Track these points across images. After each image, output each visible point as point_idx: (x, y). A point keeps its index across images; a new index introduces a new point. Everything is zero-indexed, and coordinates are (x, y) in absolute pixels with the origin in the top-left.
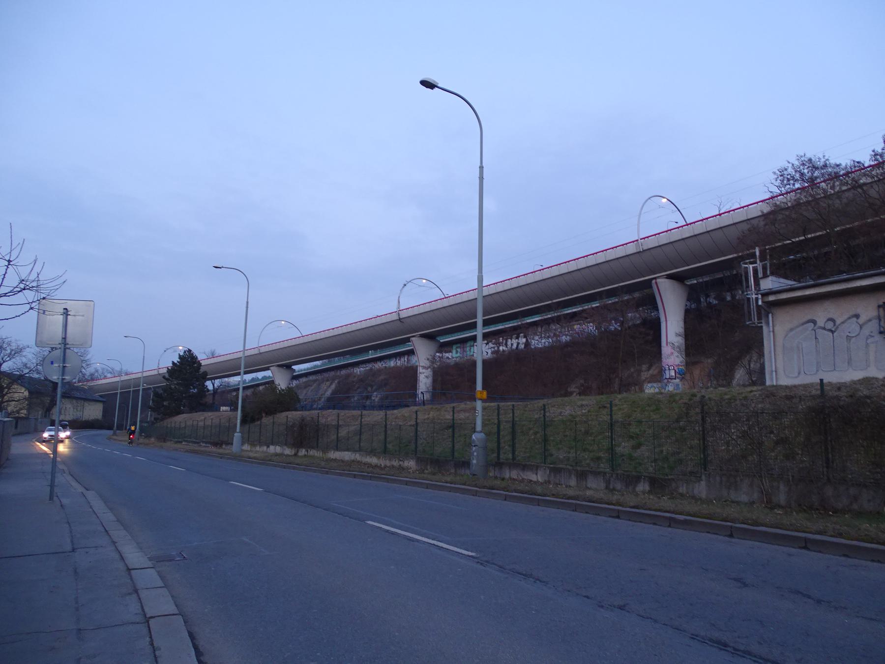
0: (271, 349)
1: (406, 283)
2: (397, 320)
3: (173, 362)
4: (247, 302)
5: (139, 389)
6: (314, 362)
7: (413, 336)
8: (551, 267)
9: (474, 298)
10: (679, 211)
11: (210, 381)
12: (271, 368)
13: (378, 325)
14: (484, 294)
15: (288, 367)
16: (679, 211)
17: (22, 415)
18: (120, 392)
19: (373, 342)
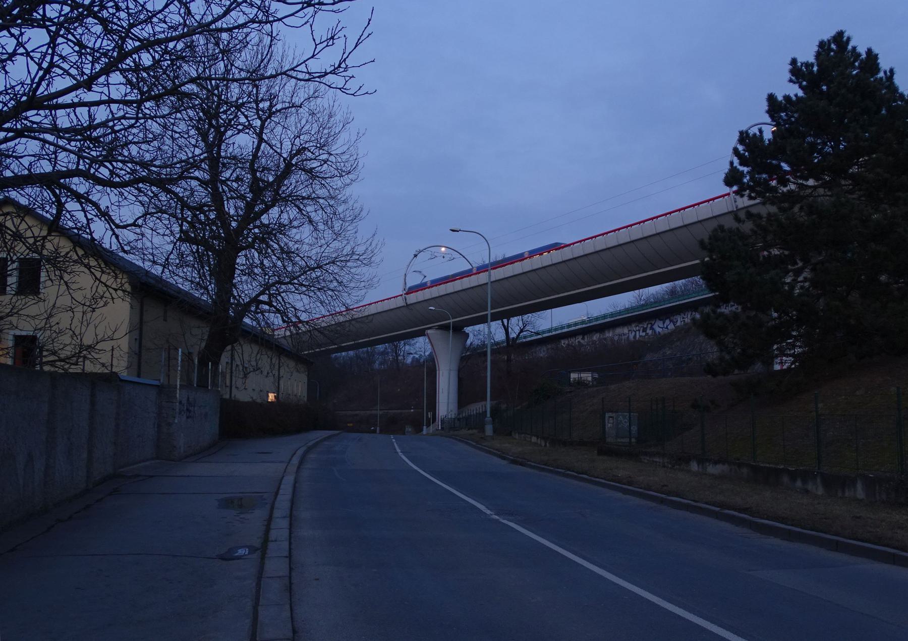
0: (380, 310)
1: (416, 253)
2: (403, 306)
3: (794, 62)
4: (372, 13)
5: (487, 314)
6: (650, 288)
7: (430, 328)
8: (713, 199)
9: (486, 282)
10: (464, 257)
11: (500, 322)
12: (429, 331)
13: (472, 288)
14: (492, 280)
15: (458, 330)
16: (464, 257)
17: (276, 320)
18: (491, 313)
19: (409, 329)
